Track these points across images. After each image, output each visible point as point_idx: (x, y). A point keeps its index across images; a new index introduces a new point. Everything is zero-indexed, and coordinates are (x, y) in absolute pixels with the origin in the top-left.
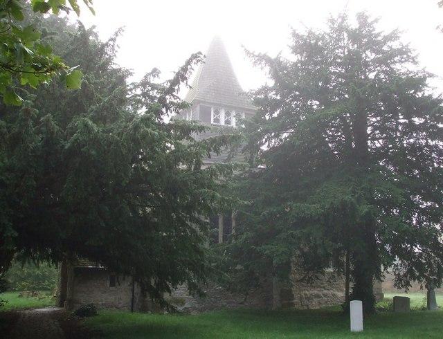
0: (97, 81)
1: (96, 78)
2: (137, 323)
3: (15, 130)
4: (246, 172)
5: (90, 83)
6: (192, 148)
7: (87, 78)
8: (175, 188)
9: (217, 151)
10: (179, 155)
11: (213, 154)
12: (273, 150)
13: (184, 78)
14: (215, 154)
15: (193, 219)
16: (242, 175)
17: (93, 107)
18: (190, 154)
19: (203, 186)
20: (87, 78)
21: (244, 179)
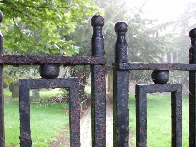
0: (115, 5)
1: (115, 4)
2: (159, 76)
3: (87, 28)
4: (181, 36)
5: (112, 6)
6: (154, 28)
7: (111, 5)
8: (147, 45)
9: (165, 28)
10: (148, 32)
11: (163, 29)
12: (85, 30)
13: (187, 14)
14: (164, 30)
15: (156, 57)
16: (180, 37)
17: (113, 16)
18: (153, 31)
19: (159, 43)
20: (111, 5)
21: (181, 39)
